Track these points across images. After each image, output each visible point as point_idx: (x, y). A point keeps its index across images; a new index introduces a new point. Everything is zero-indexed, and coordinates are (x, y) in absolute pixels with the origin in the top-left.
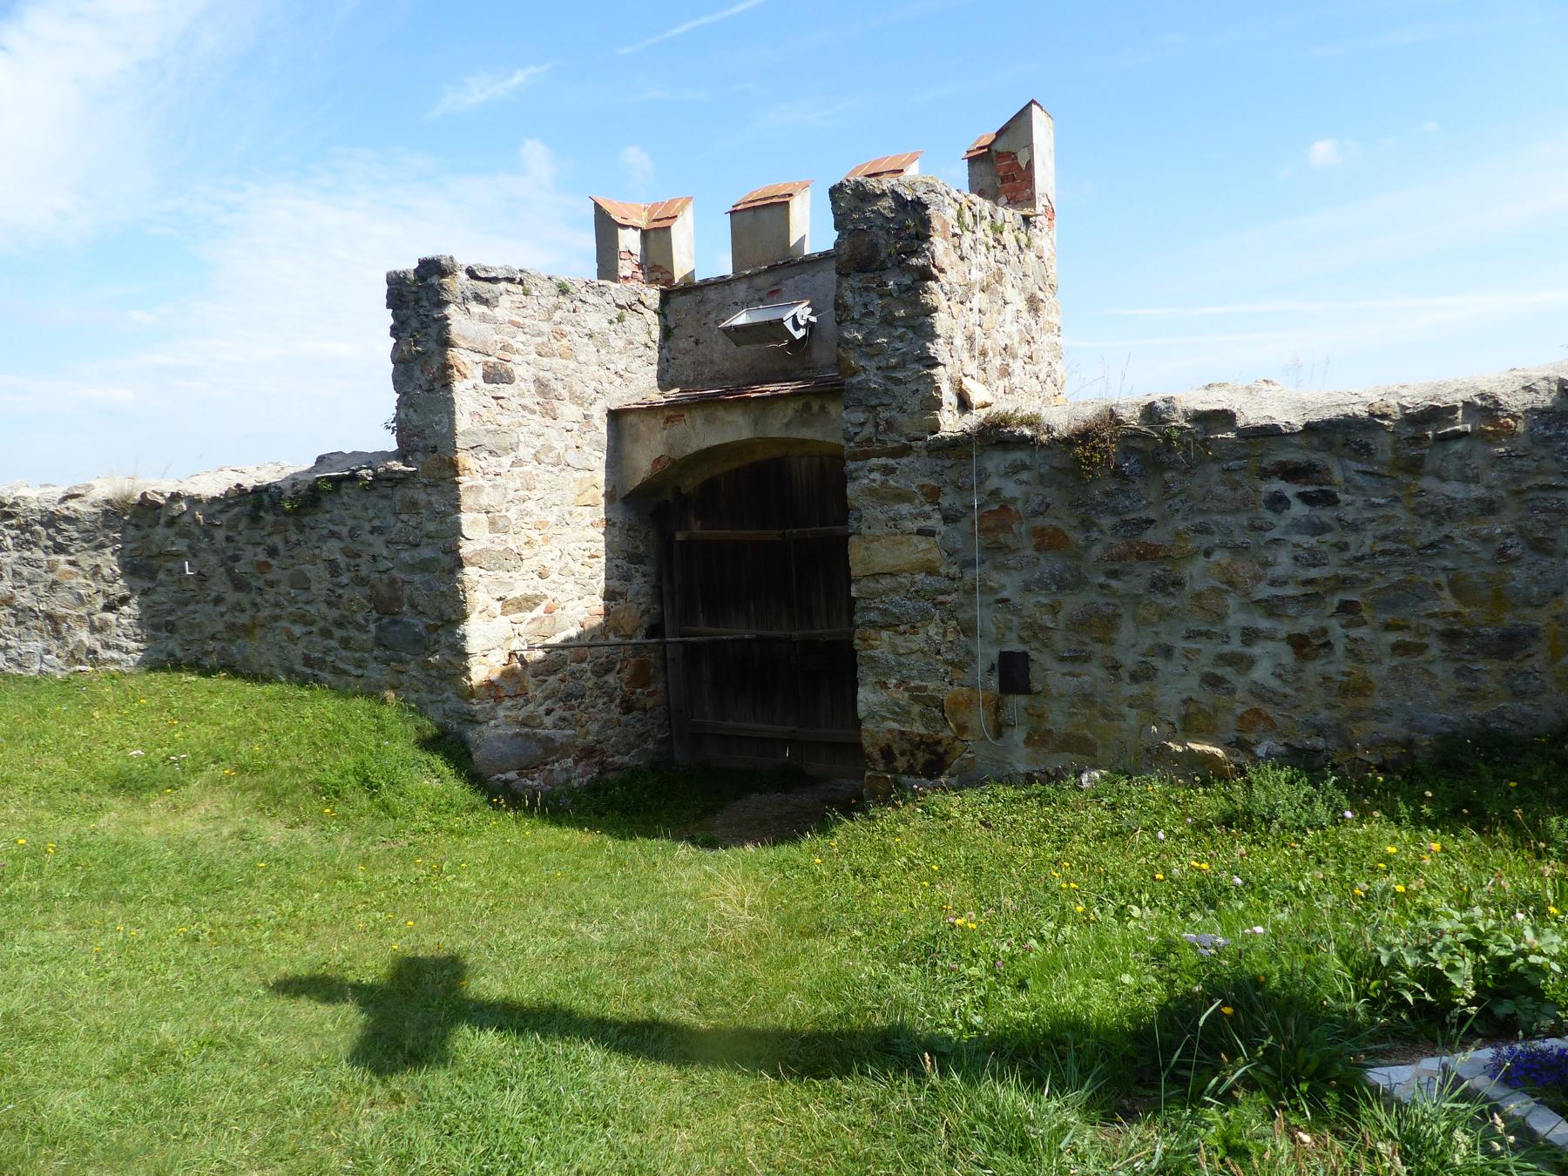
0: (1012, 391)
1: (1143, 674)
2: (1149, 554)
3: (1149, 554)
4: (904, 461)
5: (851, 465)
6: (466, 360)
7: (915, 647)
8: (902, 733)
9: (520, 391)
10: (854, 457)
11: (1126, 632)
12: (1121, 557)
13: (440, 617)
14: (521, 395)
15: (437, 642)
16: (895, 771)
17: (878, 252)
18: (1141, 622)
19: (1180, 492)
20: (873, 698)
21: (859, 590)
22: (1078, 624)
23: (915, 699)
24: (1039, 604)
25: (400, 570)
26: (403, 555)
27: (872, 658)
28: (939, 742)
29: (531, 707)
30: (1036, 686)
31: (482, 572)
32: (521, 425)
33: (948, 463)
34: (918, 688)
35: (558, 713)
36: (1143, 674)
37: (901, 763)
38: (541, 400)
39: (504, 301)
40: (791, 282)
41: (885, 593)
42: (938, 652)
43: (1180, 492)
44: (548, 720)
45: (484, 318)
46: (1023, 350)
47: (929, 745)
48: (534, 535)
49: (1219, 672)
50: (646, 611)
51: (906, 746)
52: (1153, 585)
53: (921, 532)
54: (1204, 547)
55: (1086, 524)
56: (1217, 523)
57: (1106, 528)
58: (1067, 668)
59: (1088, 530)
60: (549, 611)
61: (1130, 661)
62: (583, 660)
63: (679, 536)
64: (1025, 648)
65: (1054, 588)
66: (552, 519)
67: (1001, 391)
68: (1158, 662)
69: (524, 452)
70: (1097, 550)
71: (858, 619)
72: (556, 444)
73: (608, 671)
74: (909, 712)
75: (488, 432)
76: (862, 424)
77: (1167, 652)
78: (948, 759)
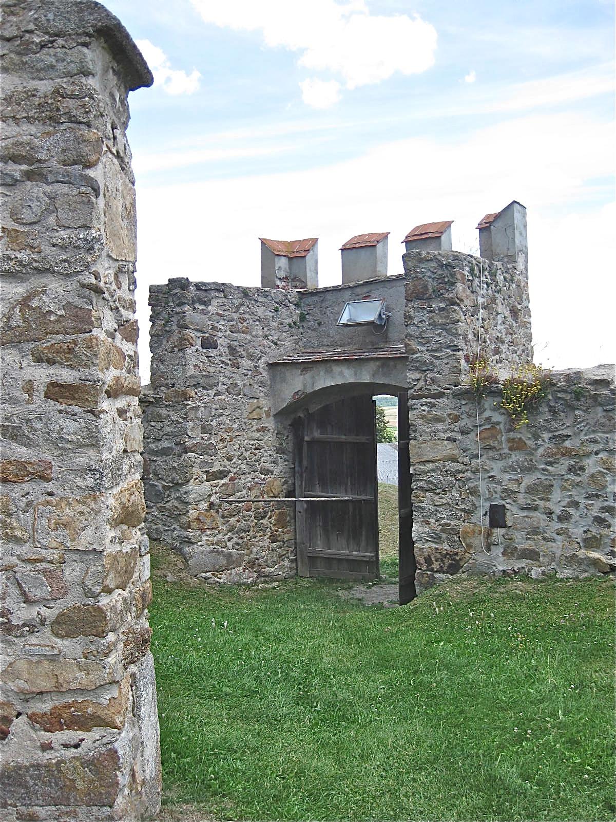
0: (501, 362)
1: (564, 517)
2: (567, 453)
3: (567, 453)
4: (440, 400)
5: (411, 402)
6: (193, 335)
7: (444, 501)
8: (437, 549)
9: (220, 353)
10: (413, 398)
11: (556, 495)
12: (553, 454)
13: (172, 482)
14: (221, 355)
15: (169, 496)
16: (432, 570)
17: (428, 290)
18: (564, 489)
19: (583, 421)
20: (421, 529)
21: (415, 470)
22: (530, 490)
23: (443, 531)
24: (510, 479)
25: (149, 454)
26: (151, 445)
27: (420, 507)
28: (457, 554)
29: (220, 536)
30: (509, 523)
31: (197, 456)
32: (220, 372)
33: (463, 402)
34: (446, 524)
35: (235, 540)
36: (564, 517)
37: (436, 566)
38: (231, 358)
39: (215, 303)
40: (377, 292)
41: (429, 472)
42: (457, 504)
43: (583, 421)
44: (230, 544)
45: (203, 312)
46: (508, 339)
47: (452, 555)
48: (225, 436)
49: (602, 516)
50: (286, 482)
51: (439, 556)
52: (570, 470)
53: (448, 439)
54: (595, 450)
55: (536, 437)
56: (601, 437)
57: (546, 439)
58: (525, 513)
59: (537, 439)
60: (232, 479)
61: (558, 510)
62: (249, 510)
63: (306, 438)
64: (503, 502)
65: (519, 470)
66: (235, 426)
67: (495, 362)
68: (572, 511)
69: (222, 388)
70: (541, 451)
71: (413, 486)
72: (239, 383)
73: (263, 518)
74: (440, 538)
75: (203, 376)
76: (418, 380)
77: (576, 504)
78: (462, 563)
